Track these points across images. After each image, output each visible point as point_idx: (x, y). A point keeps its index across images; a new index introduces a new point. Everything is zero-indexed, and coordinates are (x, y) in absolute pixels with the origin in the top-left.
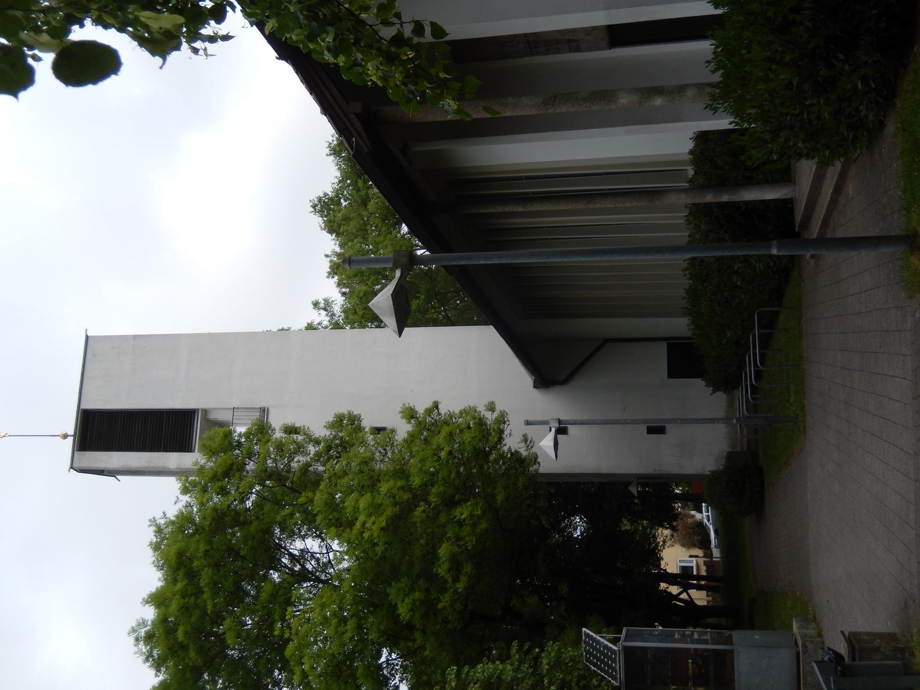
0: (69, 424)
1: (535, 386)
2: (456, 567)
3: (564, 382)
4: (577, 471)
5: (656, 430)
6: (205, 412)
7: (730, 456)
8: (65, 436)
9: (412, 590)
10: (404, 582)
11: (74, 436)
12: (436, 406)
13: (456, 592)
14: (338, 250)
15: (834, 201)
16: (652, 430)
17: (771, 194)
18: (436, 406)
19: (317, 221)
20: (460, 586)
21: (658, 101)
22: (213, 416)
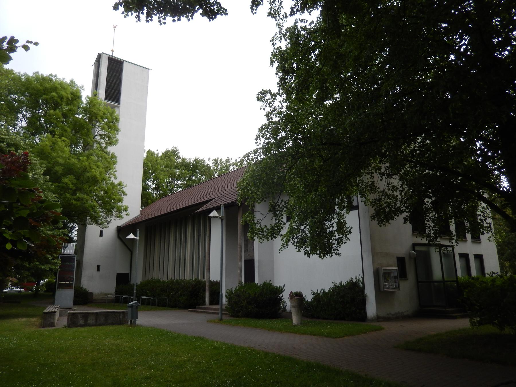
0: (118, 55)
1: (118, 226)
2: (78, 199)
3: (119, 237)
4: (373, 279)
5: (98, 268)
6: (118, 107)
7: (92, 294)
8: (112, 51)
9: (72, 184)
10: (75, 181)
11: (112, 56)
12: (126, 195)
13: (71, 199)
14: (160, 155)
15: (210, 313)
16: (99, 266)
17: (207, 300)
18: (126, 195)
19: (170, 148)
20: (73, 201)
21: (239, 271)
22: (116, 109)
